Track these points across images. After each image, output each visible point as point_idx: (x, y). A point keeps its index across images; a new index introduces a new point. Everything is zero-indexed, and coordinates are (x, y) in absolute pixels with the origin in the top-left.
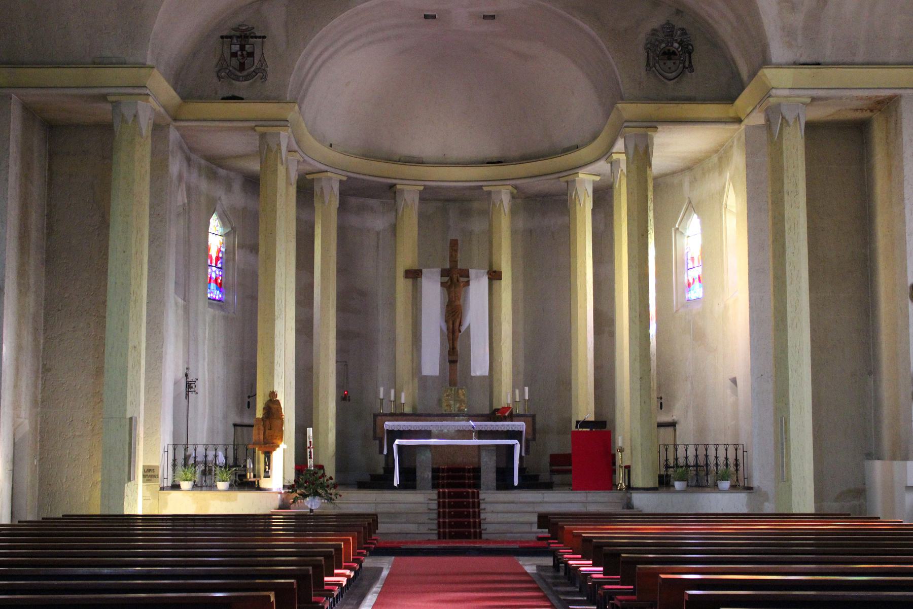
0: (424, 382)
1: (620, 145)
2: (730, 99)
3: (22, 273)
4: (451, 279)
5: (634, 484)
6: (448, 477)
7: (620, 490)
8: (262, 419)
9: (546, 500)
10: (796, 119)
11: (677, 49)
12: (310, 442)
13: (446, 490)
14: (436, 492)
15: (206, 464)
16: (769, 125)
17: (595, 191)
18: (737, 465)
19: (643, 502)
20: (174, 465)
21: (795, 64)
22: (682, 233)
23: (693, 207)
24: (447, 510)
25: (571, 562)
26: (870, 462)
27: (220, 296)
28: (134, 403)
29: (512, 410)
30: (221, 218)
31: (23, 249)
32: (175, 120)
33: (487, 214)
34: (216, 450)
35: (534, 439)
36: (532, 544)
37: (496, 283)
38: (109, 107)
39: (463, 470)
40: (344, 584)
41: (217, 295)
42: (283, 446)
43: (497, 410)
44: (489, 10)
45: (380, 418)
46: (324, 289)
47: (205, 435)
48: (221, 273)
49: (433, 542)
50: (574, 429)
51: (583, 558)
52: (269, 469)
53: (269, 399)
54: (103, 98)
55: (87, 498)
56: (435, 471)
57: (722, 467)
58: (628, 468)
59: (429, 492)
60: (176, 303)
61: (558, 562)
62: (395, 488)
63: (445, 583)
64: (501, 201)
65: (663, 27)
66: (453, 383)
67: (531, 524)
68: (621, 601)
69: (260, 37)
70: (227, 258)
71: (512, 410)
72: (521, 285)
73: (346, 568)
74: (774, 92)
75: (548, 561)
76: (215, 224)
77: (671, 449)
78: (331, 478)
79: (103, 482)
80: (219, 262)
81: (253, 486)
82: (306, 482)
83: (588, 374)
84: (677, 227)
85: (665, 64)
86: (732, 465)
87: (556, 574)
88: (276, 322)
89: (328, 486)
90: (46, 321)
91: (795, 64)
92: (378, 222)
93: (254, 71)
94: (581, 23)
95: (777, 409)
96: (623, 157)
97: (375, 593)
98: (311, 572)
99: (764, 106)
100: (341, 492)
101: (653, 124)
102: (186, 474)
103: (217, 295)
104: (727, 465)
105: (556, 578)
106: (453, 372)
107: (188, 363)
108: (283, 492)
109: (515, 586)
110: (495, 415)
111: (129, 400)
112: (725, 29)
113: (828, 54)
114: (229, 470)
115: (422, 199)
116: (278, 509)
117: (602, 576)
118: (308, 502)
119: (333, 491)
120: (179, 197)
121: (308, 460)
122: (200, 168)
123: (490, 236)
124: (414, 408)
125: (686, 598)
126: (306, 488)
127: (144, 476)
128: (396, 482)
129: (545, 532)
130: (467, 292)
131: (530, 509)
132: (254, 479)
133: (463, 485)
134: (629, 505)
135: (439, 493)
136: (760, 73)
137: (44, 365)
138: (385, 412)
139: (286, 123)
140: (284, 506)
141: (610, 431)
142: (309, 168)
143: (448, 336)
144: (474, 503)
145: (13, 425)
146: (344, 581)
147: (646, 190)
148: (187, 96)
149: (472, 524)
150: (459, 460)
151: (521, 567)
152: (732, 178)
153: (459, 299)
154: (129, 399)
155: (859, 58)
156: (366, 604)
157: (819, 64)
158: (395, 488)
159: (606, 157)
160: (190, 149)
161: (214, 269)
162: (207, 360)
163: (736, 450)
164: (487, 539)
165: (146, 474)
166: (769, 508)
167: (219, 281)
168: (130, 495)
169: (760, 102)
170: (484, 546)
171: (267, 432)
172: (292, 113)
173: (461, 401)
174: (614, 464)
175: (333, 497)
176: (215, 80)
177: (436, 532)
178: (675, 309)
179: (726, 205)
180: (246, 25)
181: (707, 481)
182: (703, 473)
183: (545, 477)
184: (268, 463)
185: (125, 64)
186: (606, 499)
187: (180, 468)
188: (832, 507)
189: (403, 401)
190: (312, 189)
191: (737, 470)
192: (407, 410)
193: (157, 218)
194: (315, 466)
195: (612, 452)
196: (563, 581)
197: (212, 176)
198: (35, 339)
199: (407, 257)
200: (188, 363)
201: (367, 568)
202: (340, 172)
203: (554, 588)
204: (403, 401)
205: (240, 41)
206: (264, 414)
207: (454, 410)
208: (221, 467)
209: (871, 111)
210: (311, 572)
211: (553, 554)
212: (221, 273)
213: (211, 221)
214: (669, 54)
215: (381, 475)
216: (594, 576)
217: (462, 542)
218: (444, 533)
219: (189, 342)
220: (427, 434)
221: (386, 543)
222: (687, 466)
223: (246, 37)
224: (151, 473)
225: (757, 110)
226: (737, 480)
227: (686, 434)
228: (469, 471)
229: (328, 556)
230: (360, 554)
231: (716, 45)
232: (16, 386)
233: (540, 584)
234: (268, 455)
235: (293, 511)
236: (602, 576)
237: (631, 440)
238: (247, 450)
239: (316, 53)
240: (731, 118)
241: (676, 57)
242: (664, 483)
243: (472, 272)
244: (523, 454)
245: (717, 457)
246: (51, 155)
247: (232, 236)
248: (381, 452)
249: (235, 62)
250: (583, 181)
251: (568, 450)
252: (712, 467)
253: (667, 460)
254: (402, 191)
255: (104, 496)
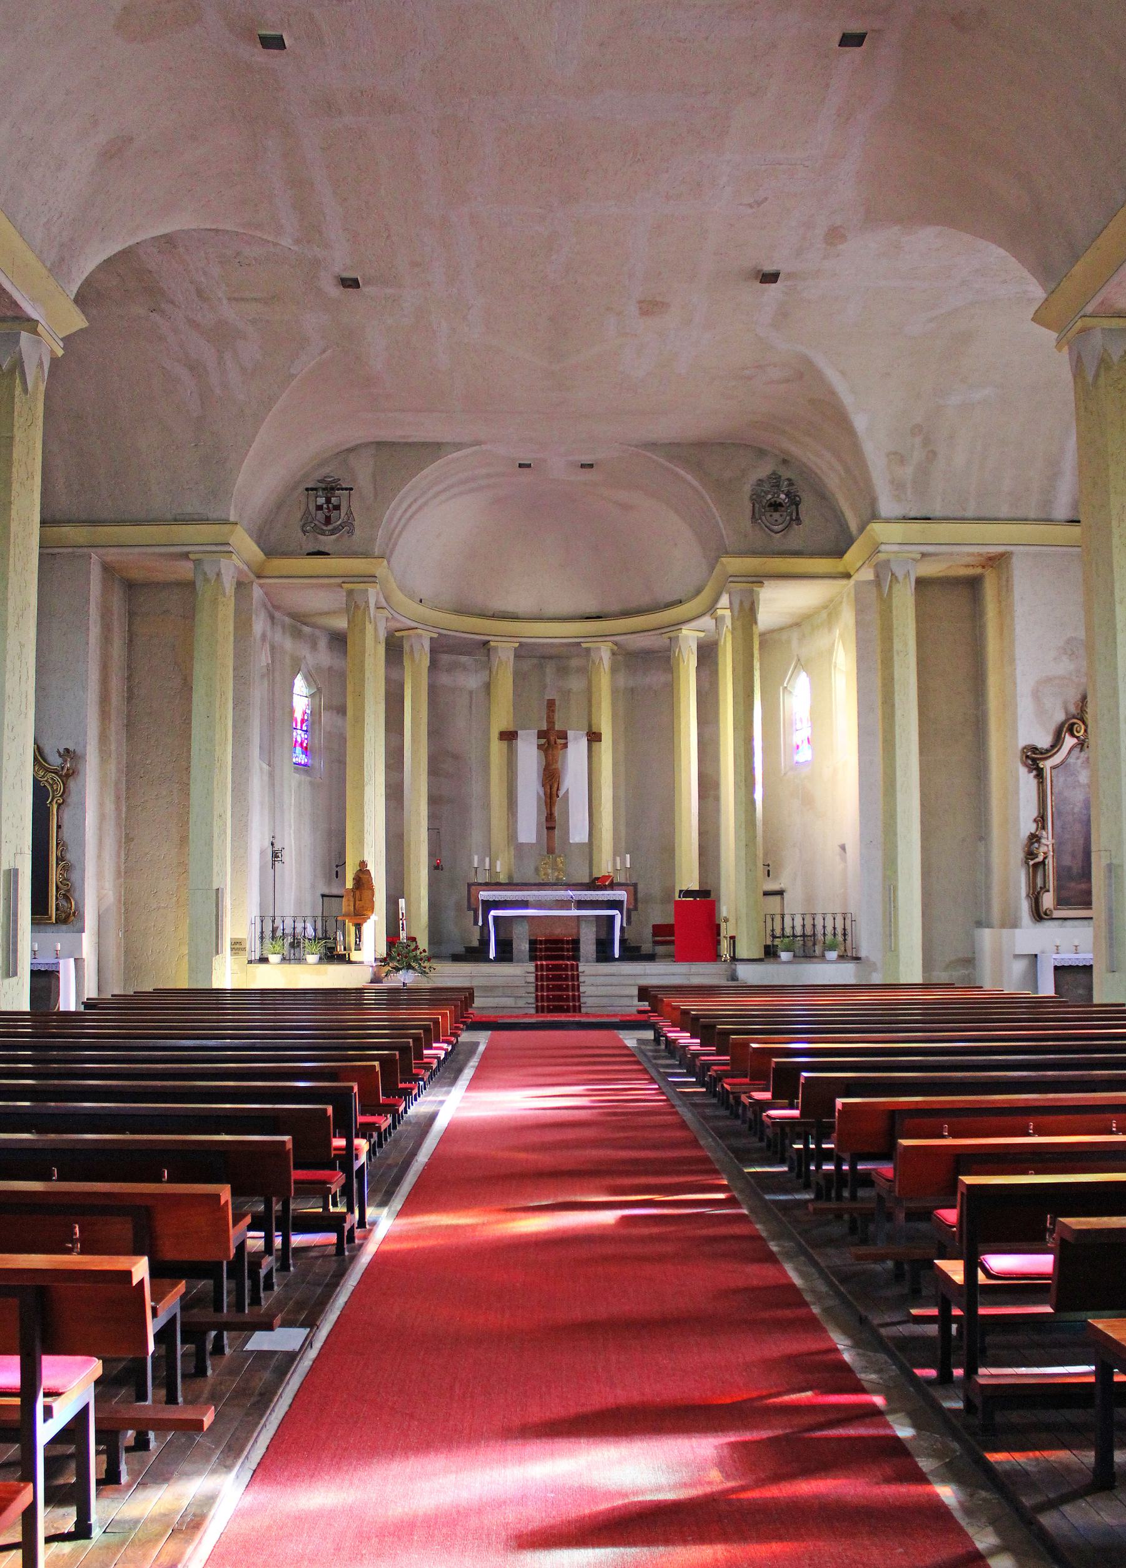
0: (520, 849)
1: (724, 600)
2: (840, 553)
3: (103, 738)
4: (549, 742)
5: (738, 956)
6: (547, 950)
7: (725, 961)
8: (352, 890)
9: (648, 972)
10: (905, 575)
11: (784, 501)
12: (403, 913)
13: (544, 963)
14: (534, 965)
15: (294, 936)
16: (878, 582)
17: (700, 648)
18: (845, 935)
19: (748, 974)
20: (262, 938)
21: (904, 518)
22: (790, 692)
23: (801, 664)
24: (545, 983)
25: (669, 1035)
26: (979, 930)
27: (306, 760)
28: (221, 874)
29: (612, 879)
30: (306, 679)
31: (104, 715)
32: (259, 577)
33: (586, 671)
34: (305, 922)
35: (636, 909)
36: (633, 1018)
37: (595, 745)
38: (190, 565)
39: (561, 941)
40: (442, 1057)
41: (302, 759)
42: (373, 918)
43: (597, 879)
44: (587, 459)
45: (473, 887)
46: (414, 752)
47: (292, 906)
48: (306, 736)
49: (531, 1016)
50: (677, 898)
51: (682, 1030)
52: (360, 941)
53: (359, 868)
54: (185, 556)
55: (173, 972)
56: (533, 943)
57: (829, 937)
58: (733, 938)
59: (527, 964)
60: (261, 769)
61: (658, 1035)
62: (491, 961)
63: (541, 1057)
64: (601, 659)
65: (769, 477)
66: (551, 850)
67: (632, 996)
68: (715, 1071)
69: (346, 489)
70: (312, 721)
71: (612, 879)
72: (621, 747)
73: (443, 1042)
74: (883, 548)
75: (649, 1035)
76: (300, 685)
77: (778, 919)
78: (424, 951)
79: (190, 954)
80: (304, 724)
81: (343, 959)
82: (398, 955)
83: (693, 841)
84: (785, 685)
85: (771, 516)
86: (840, 935)
87: (657, 1047)
88: (366, 788)
89: (421, 959)
90: (128, 788)
91: (904, 518)
92: (472, 681)
93: (340, 525)
94: (682, 472)
95: (885, 877)
96: (728, 613)
97: (472, 1067)
98: (411, 1045)
99: (874, 561)
100: (434, 965)
101: (759, 579)
102: (274, 947)
103: (302, 759)
104: (835, 935)
105: (656, 1051)
106: (550, 839)
107: (274, 831)
108: (374, 965)
109: (613, 1059)
110: (595, 884)
111: (215, 871)
112: (833, 482)
113: (938, 510)
114: (318, 943)
115: (518, 656)
116: (371, 982)
117: (699, 1048)
118: (401, 975)
119: (426, 964)
120: (263, 657)
121: (401, 932)
122: (283, 627)
123: (589, 695)
124: (510, 877)
125: (700, 1024)
126: (399, 961)
127: (232, 949)
128: (492, 955)
129: (645, 1005)
130: (565, 757)
131: (633, 982)
132: (345, 952)
133: (562, 958)
134: (734, 978)
135: (537, 966)
136: (868, 528)
137: (127, 835)
138: (480, 881)
139: (373, 579)
140: (376, 979)
141: (714, 901)
142: (398, 625)
143: (546, 802)
144: (573, 975)
145: (98, 897)
146: (442, 1054)
147: (751, 648)
148: (271, 552)
149: (571, 997)
150: (558, 932)
151: (620, 1040)
152: (841, 636)
153: (557, 762)
154: (215, 869)
155: (970, 514)
156: (463, 1078)
157: (929, 519)
158: (491, 961)
159: (710, 612)
160: (277, 608)
161: (299, 732)
162: (293, 828)
163: (844, 919)
164: (587, 1013)
165: (233, 947)
166: (877, 979)
167: (305, 745)
168: (217, 968)
169: (869, 558)
170: (583, 1020)
171: (357, 902)
172: (380, 569)
173: (559, 870)
174: (719, 935)
175: (427, 970)
176: (301, 534)
177: (534, 1006)
178: (783, 772)
179: (835, 663)
180: (332, 477)
181: (814, 951)
182: (810, 944)
183: (647, 947)
184: (359, 936)
185: (207, 520)
186: (714, 971)
187: (268, 941)
188: (942, 977)
189: (498, 870)
190: (401, 647)
191: (845, 940)
192: (503, 878)
193: (241, 679)
194: (408, 938)
195: (717, 922)
196: (663, 1054)
197: (297, 634)
198: (118, 809)
199: (501, 719)
200: (274, 831)
201: (463, 1043)
202: (431, 629)
203: (654, 1061)
204: (498, 870)
205: (326, 494)
206: (354, 884)
207: (552, 879)
208: (310, 939)
209: (983, 567)
210: (411, 1045)
211: (652, 1026)
212: (306, 736)
213: (296, 681)
214: (776, 506)
215: (476, 947)
216: (692, 1048)
217: (561, 1016)
218: (543, 1006)
219: (275, 808)
220: (524, 904)
221: (483, 1017)
222: (794, 936)
223: (332, 489)
224: (238, 946)
225: (866, 566)
226: (845, 950)
227: (794, 904)
228: (568, 942)
229: (427, 1029)
230: (457, 1028)
231: (823, 497)
232: (99, 857)
233: (641, 1058)
234: (358, 927)
235: (387, 984)
236: (699, 1048)
237: (736, 909)
238: (336, 921)
239: (404, 505)
240: (842, 573)
241: (783, 509)
242: (770, 953)
243: (571, 734)
244: (625, 925)
245: (824, 927)
246: (131, 614)
247: (317, 697)
248: (476, 922)
249: (320, 515)
250: (686, 637)
251: (671, 920)
252: (820, 937)
253: (773, 930)
254: (496, 648)
255: (192, 970)
